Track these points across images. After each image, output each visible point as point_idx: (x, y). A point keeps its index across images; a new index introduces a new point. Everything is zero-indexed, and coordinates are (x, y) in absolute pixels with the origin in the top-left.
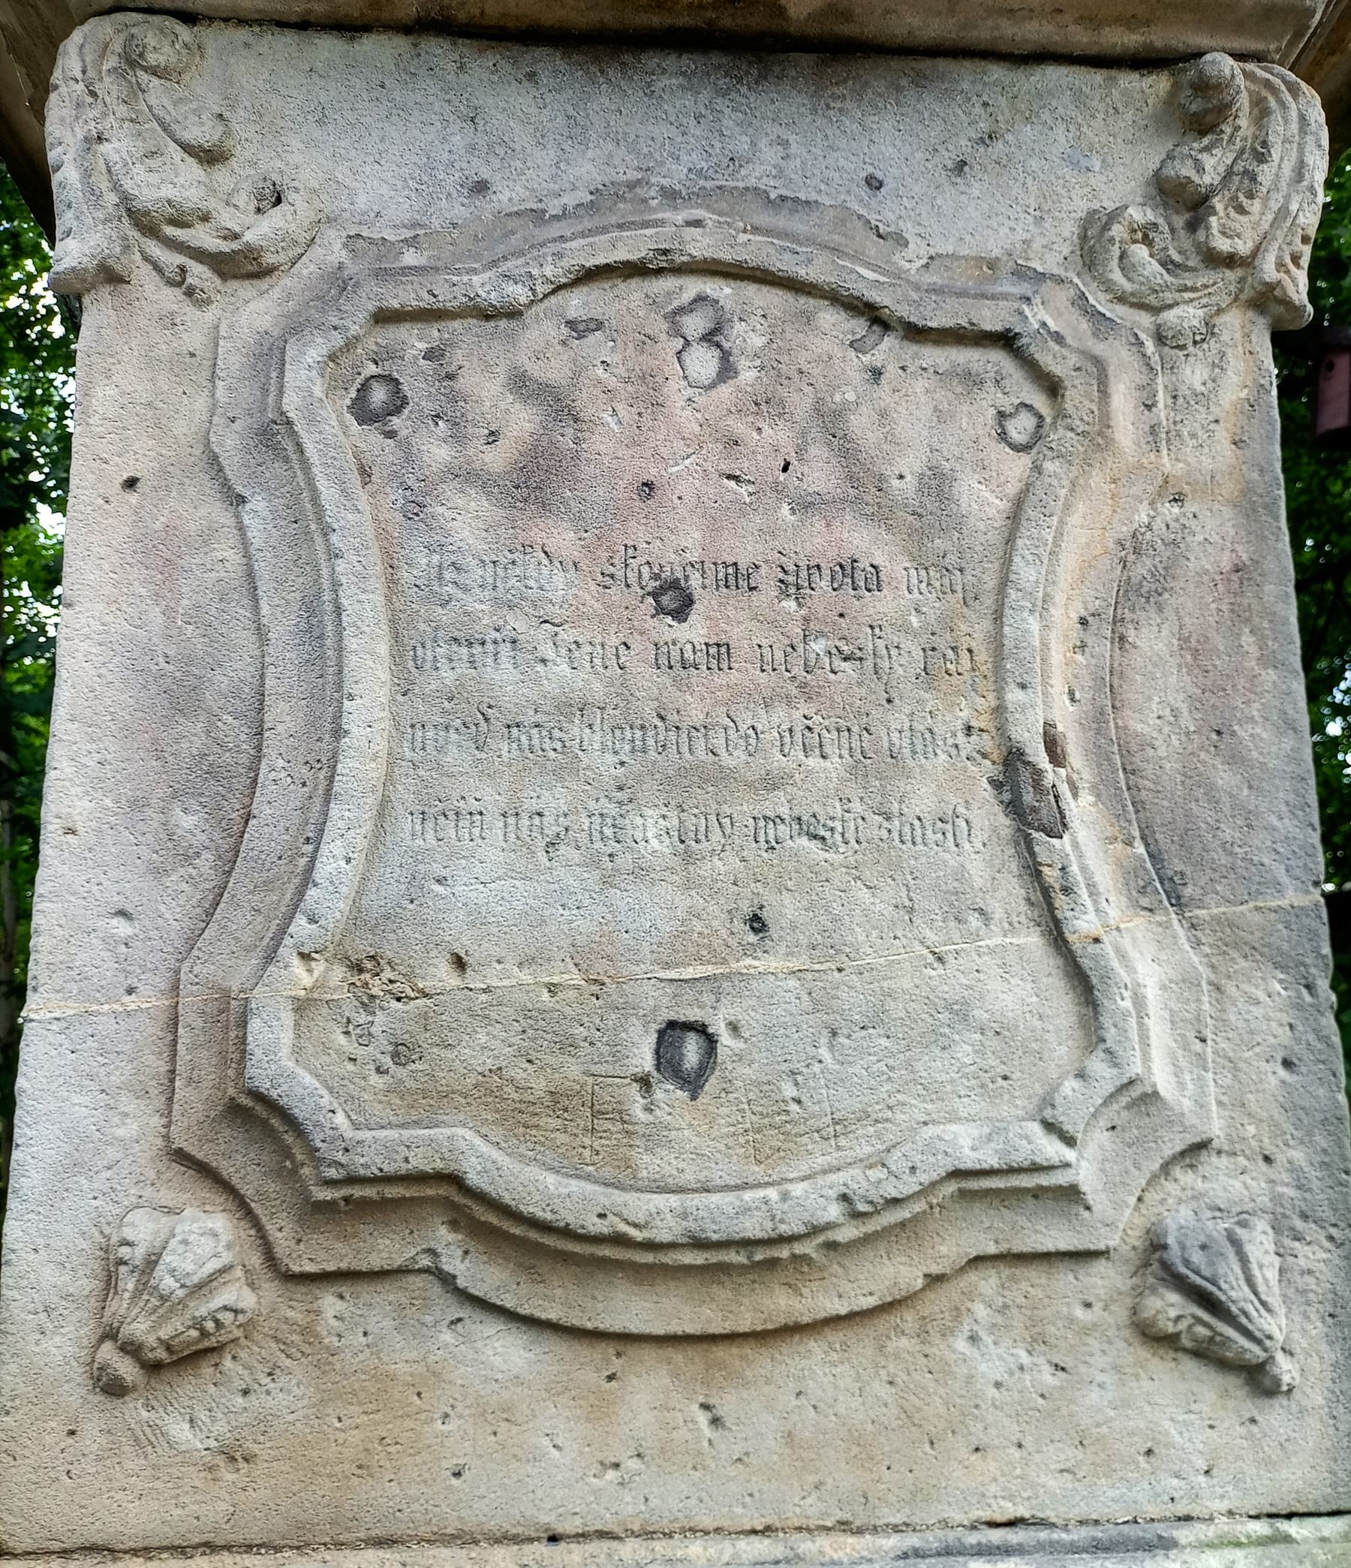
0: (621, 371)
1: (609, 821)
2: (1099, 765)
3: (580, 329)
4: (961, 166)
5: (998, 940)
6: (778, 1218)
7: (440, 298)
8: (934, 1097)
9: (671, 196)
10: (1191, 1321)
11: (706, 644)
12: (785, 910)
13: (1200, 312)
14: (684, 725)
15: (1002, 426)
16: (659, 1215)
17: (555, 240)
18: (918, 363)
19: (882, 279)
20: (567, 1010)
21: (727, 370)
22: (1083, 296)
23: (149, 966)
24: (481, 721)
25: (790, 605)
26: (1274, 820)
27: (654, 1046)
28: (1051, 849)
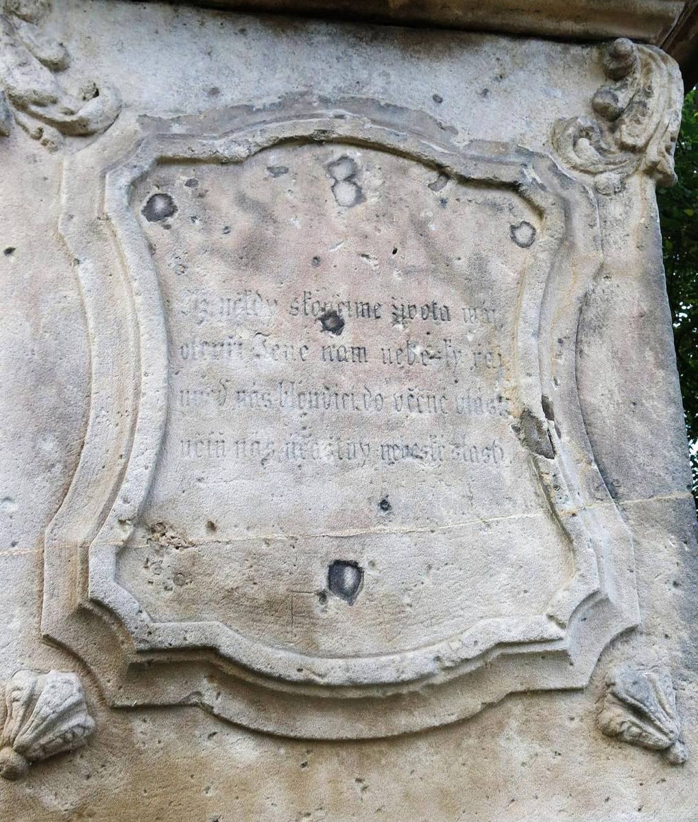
0: (300, 195)
1: (298, 447)
2: (572, 420)
3: (276, 172)
4: (485, 92)
5: (520, 515)
6: (401, 670)
7: (196, 152)
8: (487, 603)
9: (325, 101)
10: (629, 724)
11: (352, 348)
12: (399, 499)
13: (618, 176)
14: (340, 393)
15: (512, 233)
16: (334, 671)
17: (260, 123)
18: (466, 197)
19: (446, 152)
20: (277, 554)
21: (360, 197)
22: (555, 165)
23: (26, 530)
24: (222, 389)
25: (400, 327)
26: (665, 452)
27: (327, 575)
28: (548, 465)
